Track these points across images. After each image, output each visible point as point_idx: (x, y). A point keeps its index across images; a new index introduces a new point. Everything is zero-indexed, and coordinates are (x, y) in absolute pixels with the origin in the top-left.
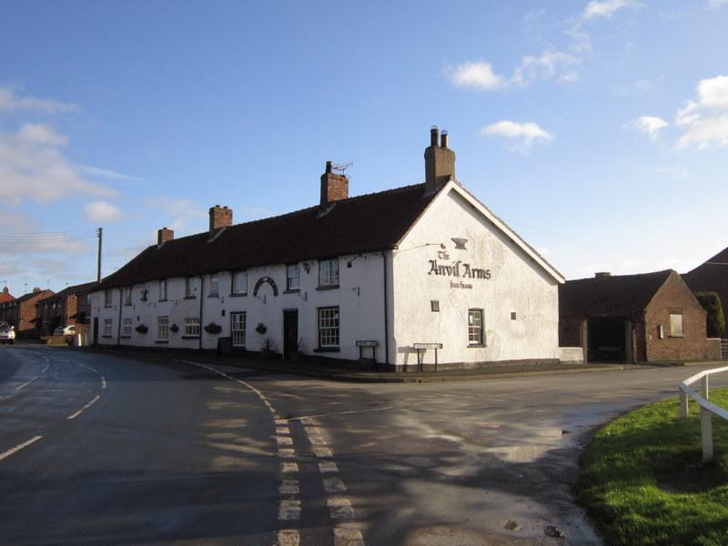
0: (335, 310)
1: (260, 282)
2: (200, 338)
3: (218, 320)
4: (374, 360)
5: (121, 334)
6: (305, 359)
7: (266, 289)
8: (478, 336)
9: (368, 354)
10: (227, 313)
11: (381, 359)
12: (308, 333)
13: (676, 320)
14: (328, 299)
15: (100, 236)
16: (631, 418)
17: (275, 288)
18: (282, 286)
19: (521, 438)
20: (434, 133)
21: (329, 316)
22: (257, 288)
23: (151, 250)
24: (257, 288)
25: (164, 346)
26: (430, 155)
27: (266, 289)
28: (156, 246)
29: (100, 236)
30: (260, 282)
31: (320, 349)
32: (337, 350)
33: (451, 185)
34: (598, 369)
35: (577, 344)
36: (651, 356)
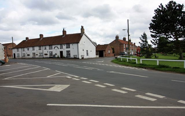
0: (62, 52)
1: (55, 47)
2: (43, 56)
3: (47, 53)
4: (9, 57)
5: (23, 56)
6: (65, 58)
7: (56, 48)
8: (28, 49)
9: (75, 57)
10: (49, 52)
11: (77, 57)
12: (65, 54)
13: (109, 52)
14: (68, 49)
15: (12, 38)
16: (167, 36)
17: (58, 48)
18: (59, 48)
19: (180, 38)
20: (82, 26)
21: (68, 52)
22: (54, 48)
23: (24, 41)
24: (54, 48)
25: (19, 57)
26: (81, 29)
27: (56, 48)
28: (25, 40)
29: (12, 38)
30: (55, 47)
31: (67, 57)
32: (70, 56)
33: (84, 34)
34: (56, 60)
35: (98, 55)
36: (42, 52)
